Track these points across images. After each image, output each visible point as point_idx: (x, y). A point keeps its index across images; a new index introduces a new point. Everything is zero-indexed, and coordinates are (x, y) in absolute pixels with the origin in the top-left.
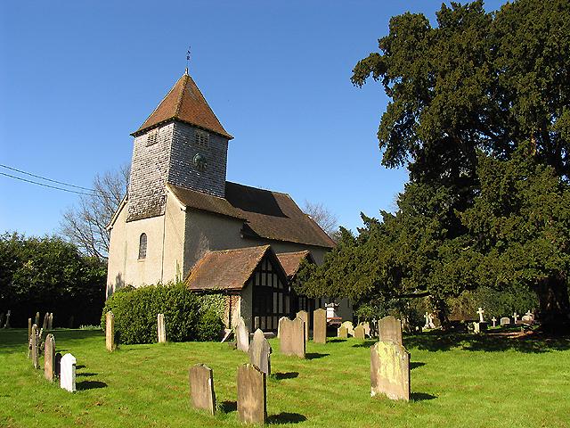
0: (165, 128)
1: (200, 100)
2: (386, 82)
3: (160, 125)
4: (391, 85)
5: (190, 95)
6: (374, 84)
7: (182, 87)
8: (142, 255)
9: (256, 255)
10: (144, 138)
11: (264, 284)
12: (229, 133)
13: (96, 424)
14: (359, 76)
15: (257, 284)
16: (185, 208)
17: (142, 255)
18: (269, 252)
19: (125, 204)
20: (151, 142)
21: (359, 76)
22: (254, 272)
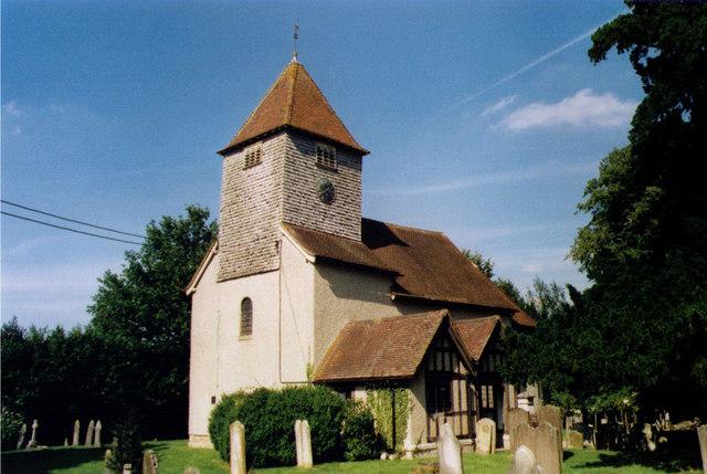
0: (274, 141)
1: (317, 99)
2: (634, 58)
3: (264, 137)
4: (643, 61)
5: (306, 92)
6: (618, 62)
7: (292, 80)
8: (246, 327)
9: (428, 326)
10: (240, 157)
11: (439, 368)
12: (362, 144)
13: (92, 422)
14: (597, 53)
15: (431, 368)
16: (313, 259)
17: (246, 327)
18: (445, 320)
19: (214, 254)
20: (253, 162)
21: (597, 53)
22: (428, 351)
